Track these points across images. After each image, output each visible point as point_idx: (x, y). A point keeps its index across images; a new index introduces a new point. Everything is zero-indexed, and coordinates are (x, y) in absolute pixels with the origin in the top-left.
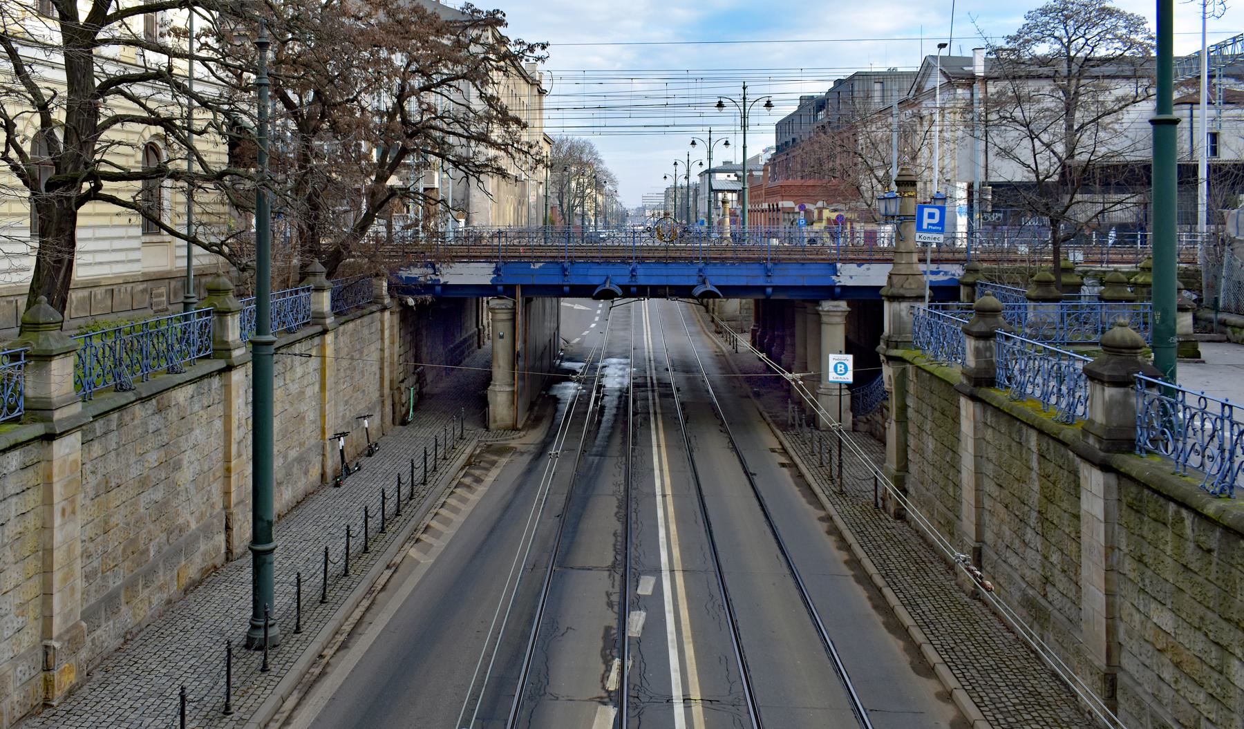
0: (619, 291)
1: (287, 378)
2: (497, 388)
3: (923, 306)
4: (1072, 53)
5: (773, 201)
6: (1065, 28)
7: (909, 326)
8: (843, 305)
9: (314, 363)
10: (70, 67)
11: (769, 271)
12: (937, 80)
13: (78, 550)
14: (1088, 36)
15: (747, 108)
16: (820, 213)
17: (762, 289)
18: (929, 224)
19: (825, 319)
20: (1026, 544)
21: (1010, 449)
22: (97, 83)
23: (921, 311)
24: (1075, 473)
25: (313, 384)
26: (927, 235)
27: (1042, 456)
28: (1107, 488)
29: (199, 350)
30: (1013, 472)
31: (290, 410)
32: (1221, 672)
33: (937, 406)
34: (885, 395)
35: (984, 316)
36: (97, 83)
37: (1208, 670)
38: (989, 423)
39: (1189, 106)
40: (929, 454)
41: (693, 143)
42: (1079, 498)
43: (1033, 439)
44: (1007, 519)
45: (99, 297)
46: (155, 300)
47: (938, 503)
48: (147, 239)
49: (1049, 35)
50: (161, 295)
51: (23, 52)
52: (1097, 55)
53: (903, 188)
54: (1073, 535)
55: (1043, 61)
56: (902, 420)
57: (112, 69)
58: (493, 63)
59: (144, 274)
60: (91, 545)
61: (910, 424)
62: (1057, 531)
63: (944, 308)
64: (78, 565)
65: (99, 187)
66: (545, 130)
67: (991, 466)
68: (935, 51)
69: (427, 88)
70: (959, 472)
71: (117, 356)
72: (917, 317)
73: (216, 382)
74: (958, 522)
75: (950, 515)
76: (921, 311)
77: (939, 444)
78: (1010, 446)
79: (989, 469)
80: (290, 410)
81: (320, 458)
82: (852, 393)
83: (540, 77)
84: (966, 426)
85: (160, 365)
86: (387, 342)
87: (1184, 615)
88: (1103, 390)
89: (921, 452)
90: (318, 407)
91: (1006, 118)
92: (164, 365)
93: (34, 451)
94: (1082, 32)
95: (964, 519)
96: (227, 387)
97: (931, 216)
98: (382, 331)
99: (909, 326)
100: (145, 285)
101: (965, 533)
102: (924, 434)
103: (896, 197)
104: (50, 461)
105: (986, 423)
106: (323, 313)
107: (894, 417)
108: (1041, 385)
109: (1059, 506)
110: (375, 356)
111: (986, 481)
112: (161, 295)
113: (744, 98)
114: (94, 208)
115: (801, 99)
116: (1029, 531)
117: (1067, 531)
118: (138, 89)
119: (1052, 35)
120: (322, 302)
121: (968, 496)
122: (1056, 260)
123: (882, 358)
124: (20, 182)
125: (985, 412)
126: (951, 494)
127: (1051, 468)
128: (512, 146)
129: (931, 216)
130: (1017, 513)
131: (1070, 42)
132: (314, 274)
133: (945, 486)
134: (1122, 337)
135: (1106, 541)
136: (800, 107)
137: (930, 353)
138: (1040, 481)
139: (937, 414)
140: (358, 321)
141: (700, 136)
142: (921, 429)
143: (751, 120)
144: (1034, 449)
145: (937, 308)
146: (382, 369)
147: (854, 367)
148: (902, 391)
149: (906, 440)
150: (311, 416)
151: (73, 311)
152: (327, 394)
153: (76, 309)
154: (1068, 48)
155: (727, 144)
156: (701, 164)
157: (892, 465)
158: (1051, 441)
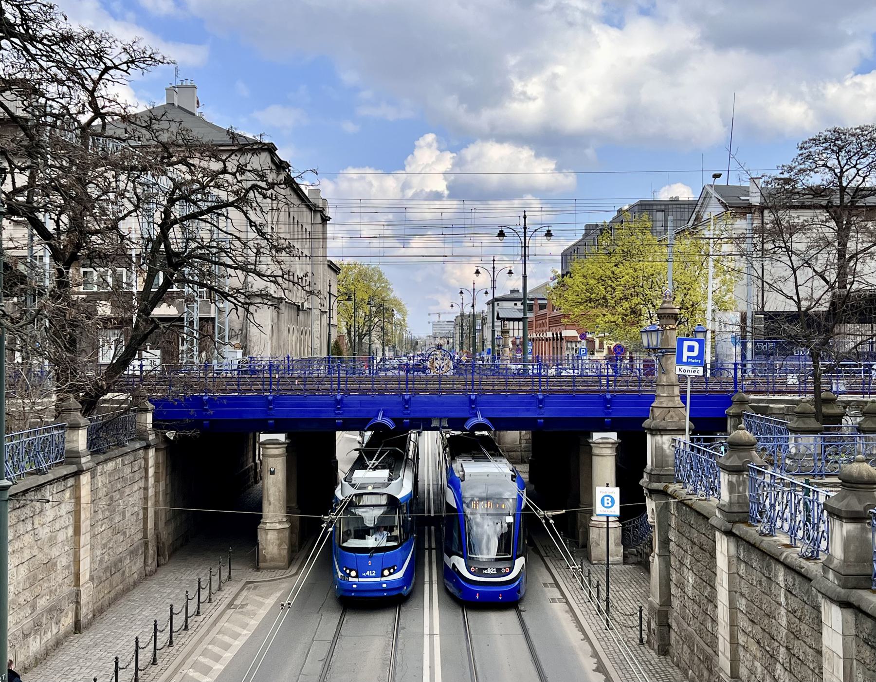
1: (36, 522)
2: (268, 526)
3: (685, 438)
4: (844, 184)
6: (838, 159)
7: (671, 460)
8: (613, 436)
9: (67, 507)
12: (714, 209)
14: (859, 167)
15: (527, 238)
18: (688, 357)
19: (596, 451)
21: (761, 584)
23: (682, 444)
24: (817, 609)
25: (66, 528)
26: (687, 368)
27: (789, 591)
28: (845, 622)
30: (764, 607)
31: (40, 556)
33: (695, 540)
34: (650, 527)
35: (739, 450)
38: (741, 558)
40: (689, 591)
41: (477, 272)
42: (821, 634)
43: (781, 575)
44: (759, 655)
47: (698, 638)
49: (823, 166)
52: (868, 185)
53: (664, 321)
54: (817, 671)
55: (817, 192)
61: (672, 558)
62: (804, 667)
63: (706, 440)
66: (328, 258)
67: (744, 601)
68: (711, 181)
69: (193, 216)
70: (716, 607)
72: (677, 450)
74: (716, 657)
75: (710, 651)
76: (682, 444)
77: (698, 579)
78: (760, 581)
79: (742, 604)
80: (40, 556)
81: (74, 606)
82: (623, 525)
83: (324, 204)
86: (151, 481)
88: (842, 526)
89: (681, 585)
90: (71, 552)
91: (781, 247)
94: (854, 162)
95: (720, 654)
97: (691, 349)
98: (146, 470)
99: (671, 460)
101: (721, 669)
102: (685, 569)
103: (658, 330)
105: (739, 558)
106: (78, 452)
107: (657, 550)
108: (789, 520)
109: (805, 642)
110: (138, 496)
111: (740, 615)
113: (525, 228)
115: (586, 226)
116: (778, 666)
117: (811, 666)
119: (825, 165)
120: (77, 441)
121: (723, 632)
122: (817, 391)
125: (738, 547)
126: (710, 629)
128: (282, 277)
129: (691, 349)
130: (768, 648)
131: (842, 172)
132: (69, 410)
133: (704, 621)
134: (860, 473)
136: (586, 235)
137: (690, 487)
138: (787, 616)
139: (696, 548)
140: (119, 460)
141: (485, 266)
142: (682, 564)
144: (782, 584)
145: (699, 440)
146: (145, 510)
147: (621, 503)
148: (664, 526)
149: (669, 574)
150: (64, 561)
152: (82, 538)
154: (840, 178)
155: (510, 272)
156: (486, 293)
157: (656, 600)
158: (796, 576)
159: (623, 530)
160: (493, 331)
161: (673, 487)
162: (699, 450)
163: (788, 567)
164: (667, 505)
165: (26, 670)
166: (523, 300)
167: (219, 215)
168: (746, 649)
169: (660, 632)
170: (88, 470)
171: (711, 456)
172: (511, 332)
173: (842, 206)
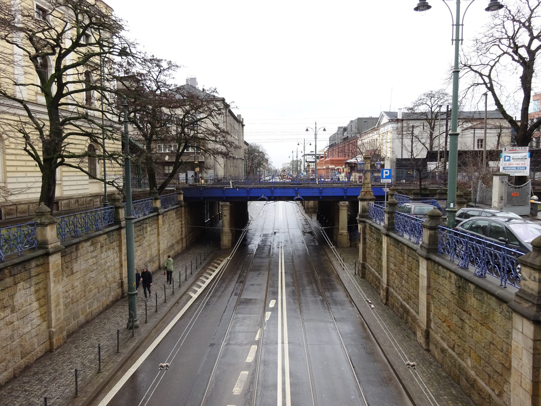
0: (267, 198)
1: (144, 232)
5: (327, 165)
8: (347, 203)
10: (50, 114)
11: (272, 191)
13: (61, 295)
16: (343, 170)
17: (319, 197)
19: (340, 208)
20: (403, 286)
22: (61, 120)
24: (418, 261)
25: (155, 234)
26: (385, 180)
29: (109, 222)
32: (462, 329)
36: (61, 120)
37: (458, 328)
39: (473, 130)
41: (298, 144)
43: (406, 248)
45: (73, 202)
46: (95, 203)
48: (91, 181)
50: (97, 202)
51: (30, 107)
55: (422, 114)
56: (365, 243)
57: (69, 115)
58: (217, 112)
59: (90, 194)
60: (67, 294)
64: (61, 301)
65: (63, 160)
71: (75, 225)
73: (115, 233)
75: (379, 276)
84: (385, 245)
85: (93, 228)
87: (451, 309)
92: (94, 227)
93: (41, 261)
96: (120, 235)
100: (91, 198)
104: (48, 263)
112: (97, 202)
114: (35, 169)
118: (78, 123)
123: (358, 221)
124: (32, 159)
127: (410, 259)
129: (386, 173)
135: (427, 285)
143: (318, 136)
145: (377, 203)
151: (62, 207)
153: (64, 207)
154: (431, 109)
155: (310, 144)
159: (350, 236)
160: (304, 166)
161: (367, 221)
162: (377, 206)
163: (408, 247)
164: (365, 226)
165: (153, 273)
166: (315, 155)
167: (202, 122)
168: (392, 275)
169: (362, 270)
170: (162, 214)
171: (382, 208)
172: (311, 166)
173: (432, 119)
